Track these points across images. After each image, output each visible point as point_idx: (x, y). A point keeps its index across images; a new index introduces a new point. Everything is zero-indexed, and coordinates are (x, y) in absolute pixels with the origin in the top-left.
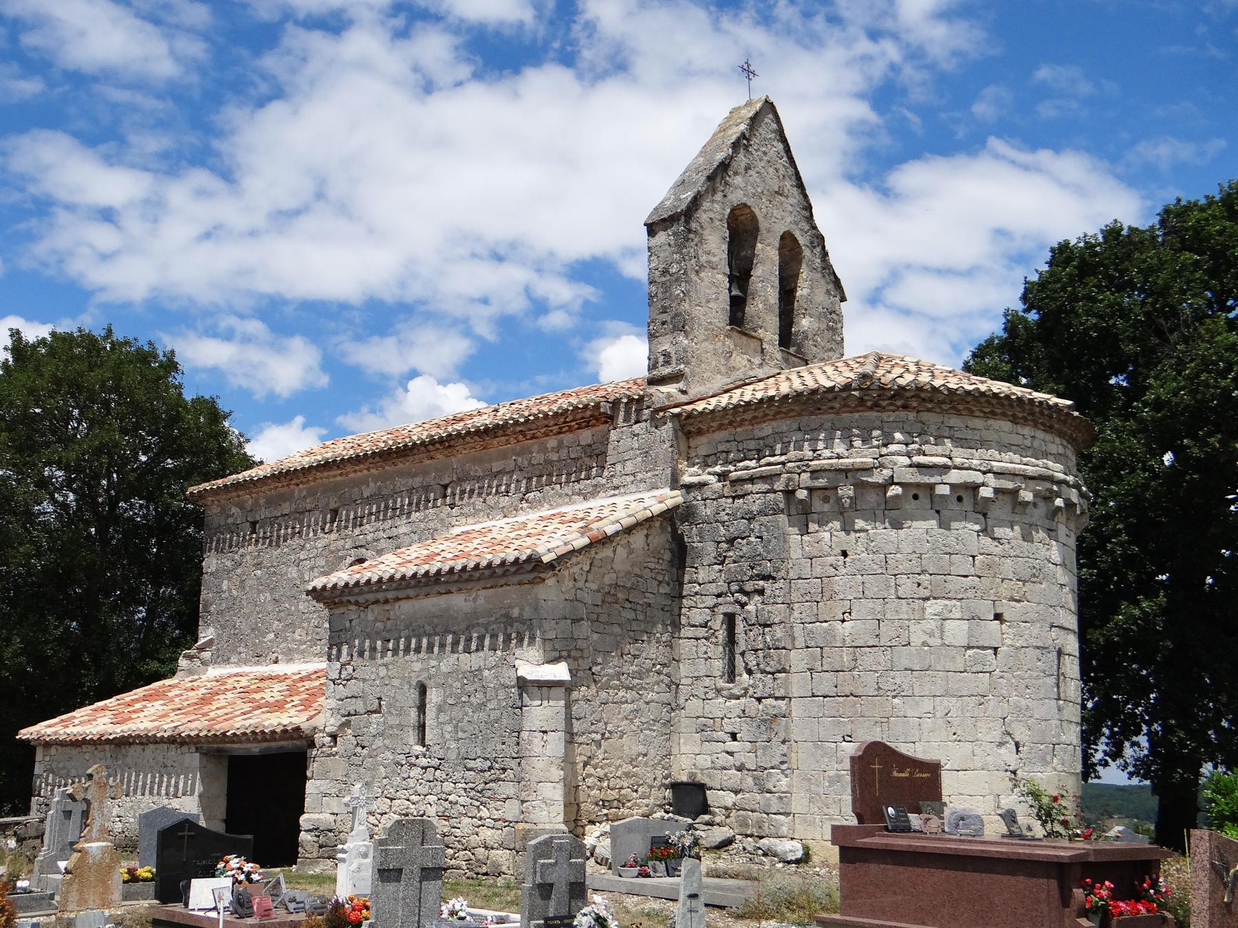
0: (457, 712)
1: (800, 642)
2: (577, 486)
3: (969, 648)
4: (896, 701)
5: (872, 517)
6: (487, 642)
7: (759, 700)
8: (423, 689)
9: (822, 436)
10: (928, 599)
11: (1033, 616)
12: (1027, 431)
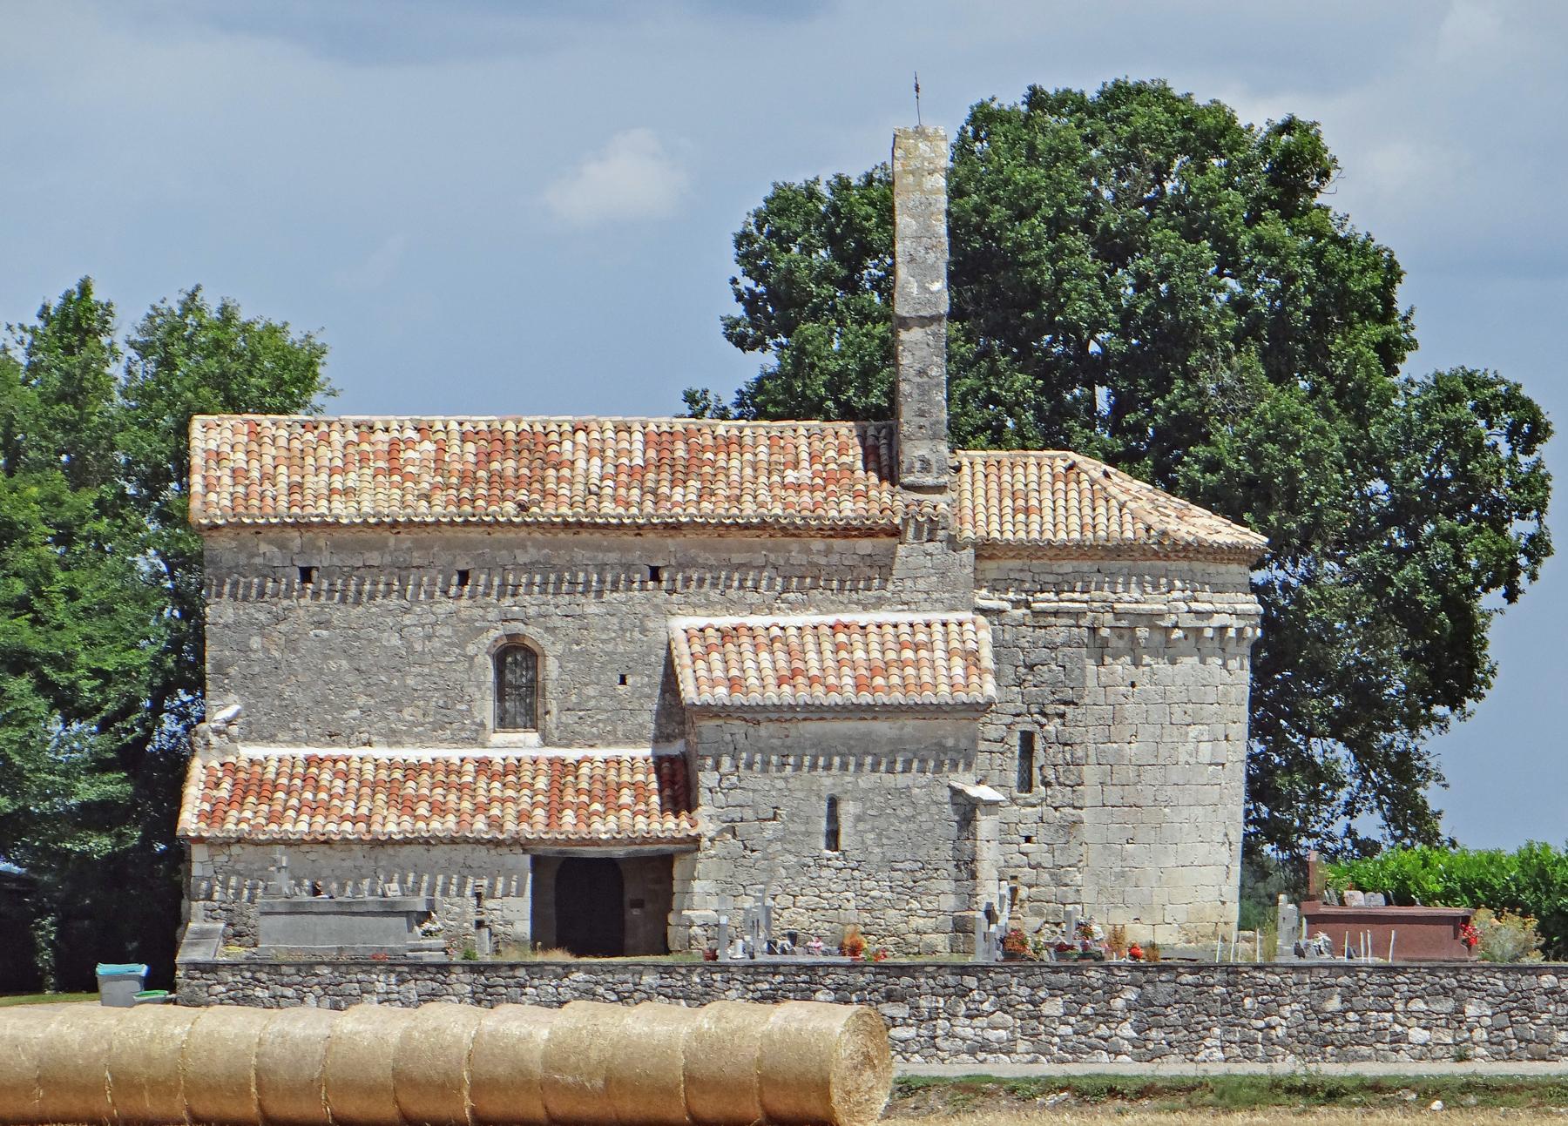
0: (882, 823)
1: (1092, 760)
2: (854, 596)
3: (1210, 764)
4: (1167, 810)
5: (1155, 654)
6: (915, 765)
7: (1056, 809)
8: (833, 803)
9: (1121, 580)
10: (1188, 725)
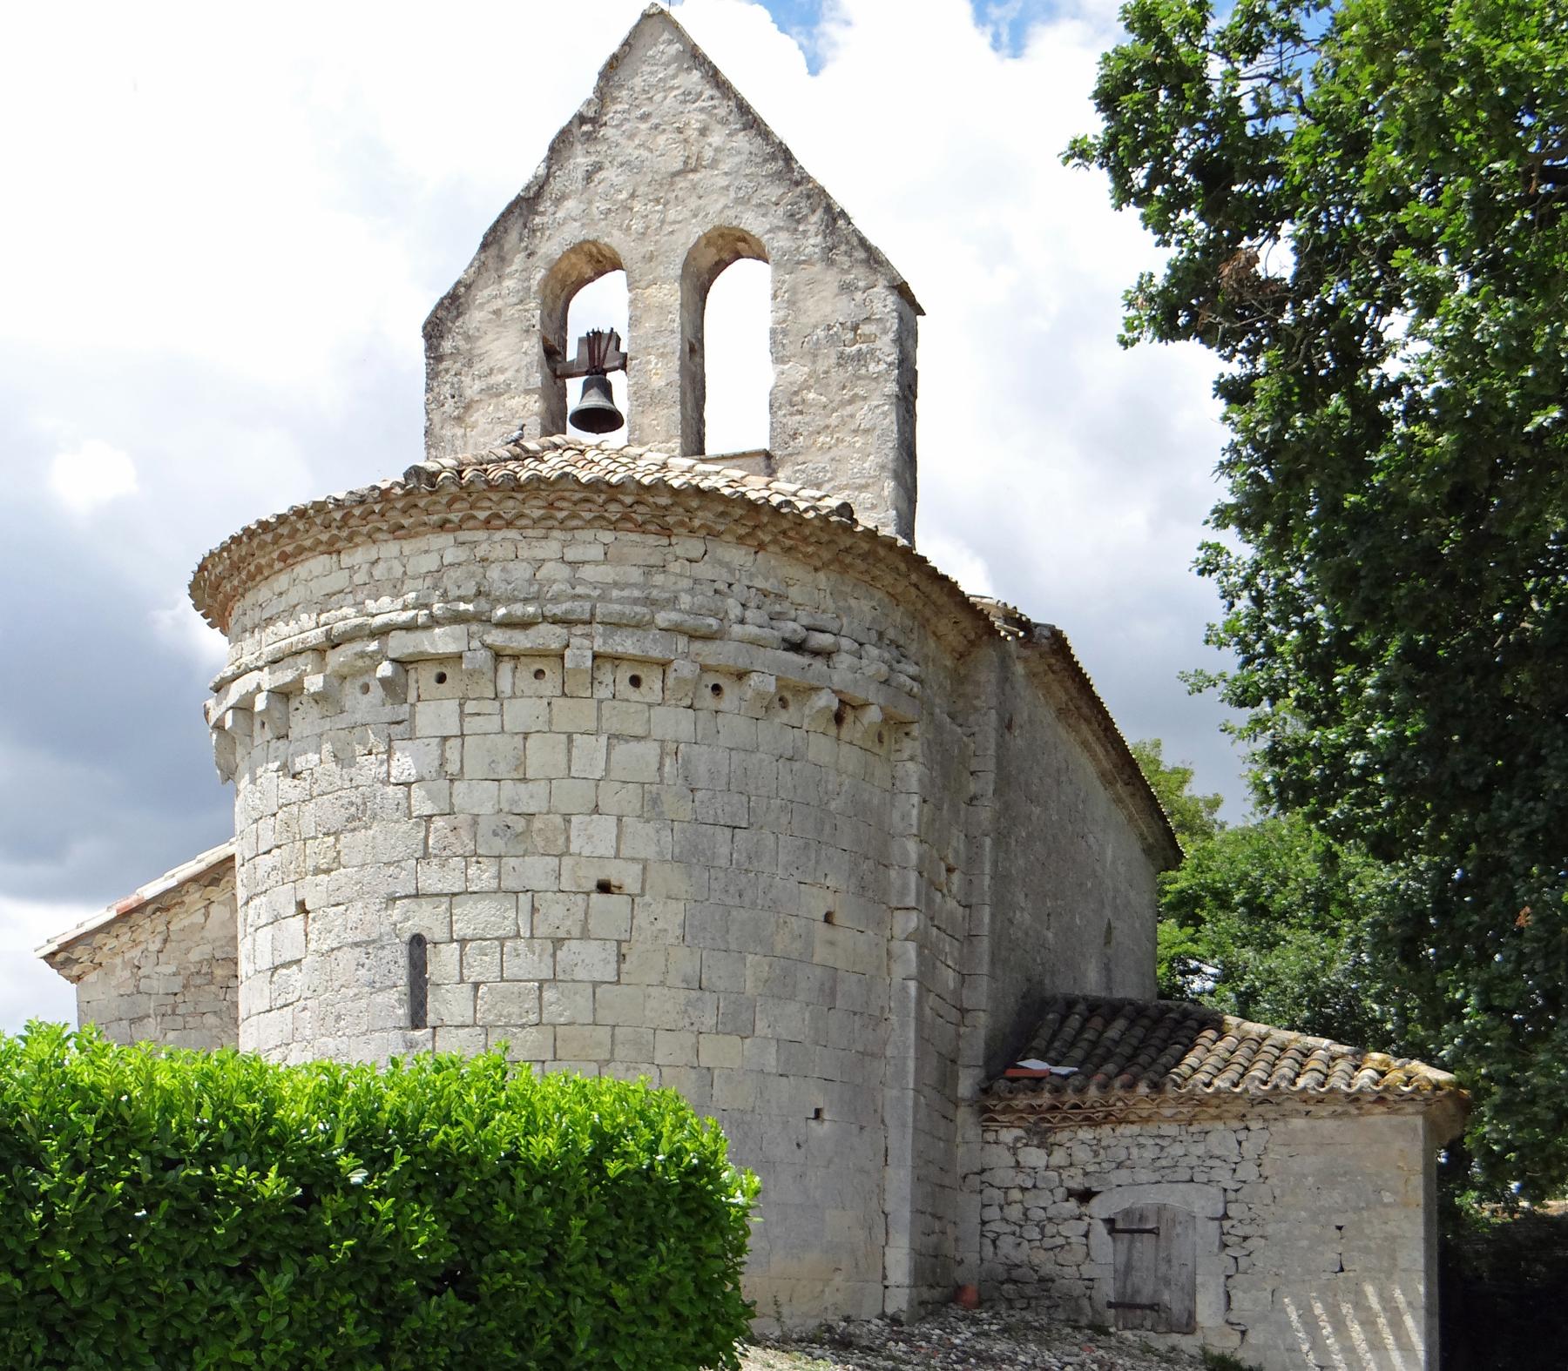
11: (348, 892)
12: (358, 556)
